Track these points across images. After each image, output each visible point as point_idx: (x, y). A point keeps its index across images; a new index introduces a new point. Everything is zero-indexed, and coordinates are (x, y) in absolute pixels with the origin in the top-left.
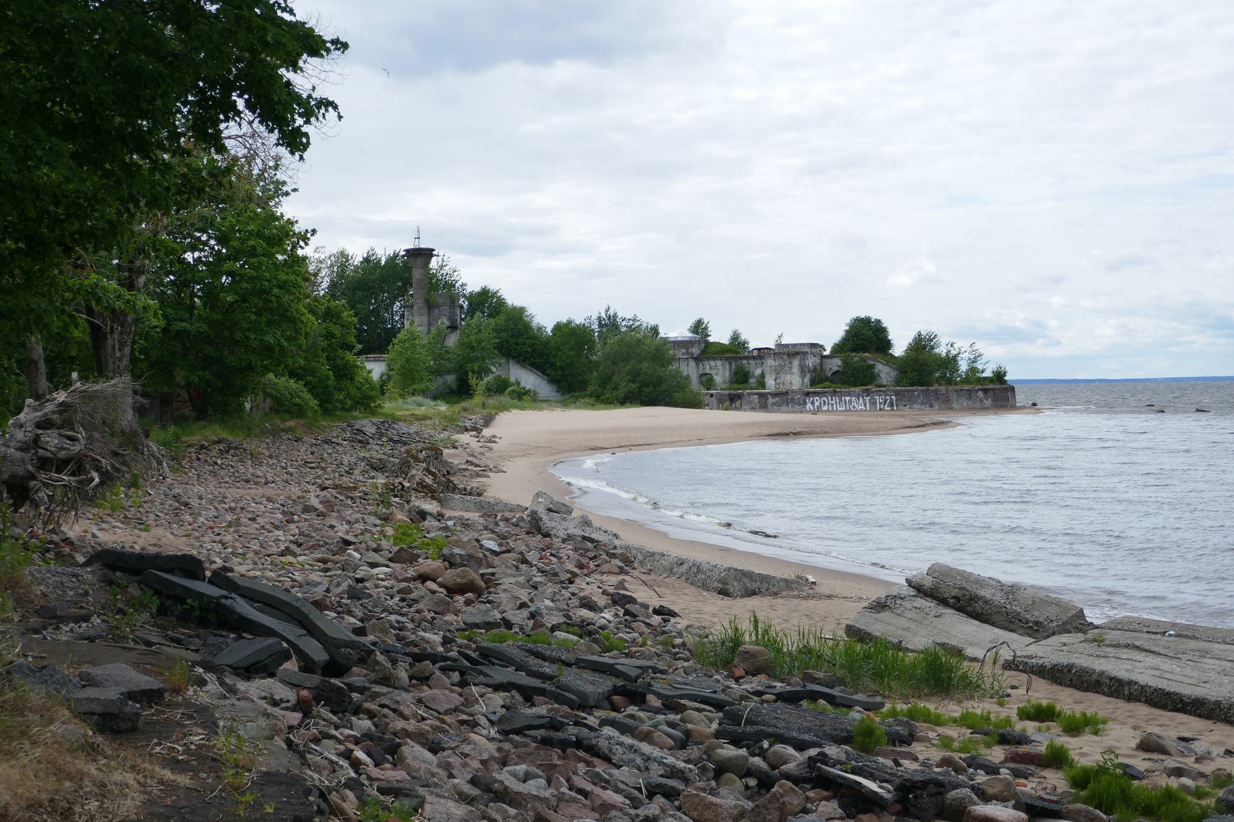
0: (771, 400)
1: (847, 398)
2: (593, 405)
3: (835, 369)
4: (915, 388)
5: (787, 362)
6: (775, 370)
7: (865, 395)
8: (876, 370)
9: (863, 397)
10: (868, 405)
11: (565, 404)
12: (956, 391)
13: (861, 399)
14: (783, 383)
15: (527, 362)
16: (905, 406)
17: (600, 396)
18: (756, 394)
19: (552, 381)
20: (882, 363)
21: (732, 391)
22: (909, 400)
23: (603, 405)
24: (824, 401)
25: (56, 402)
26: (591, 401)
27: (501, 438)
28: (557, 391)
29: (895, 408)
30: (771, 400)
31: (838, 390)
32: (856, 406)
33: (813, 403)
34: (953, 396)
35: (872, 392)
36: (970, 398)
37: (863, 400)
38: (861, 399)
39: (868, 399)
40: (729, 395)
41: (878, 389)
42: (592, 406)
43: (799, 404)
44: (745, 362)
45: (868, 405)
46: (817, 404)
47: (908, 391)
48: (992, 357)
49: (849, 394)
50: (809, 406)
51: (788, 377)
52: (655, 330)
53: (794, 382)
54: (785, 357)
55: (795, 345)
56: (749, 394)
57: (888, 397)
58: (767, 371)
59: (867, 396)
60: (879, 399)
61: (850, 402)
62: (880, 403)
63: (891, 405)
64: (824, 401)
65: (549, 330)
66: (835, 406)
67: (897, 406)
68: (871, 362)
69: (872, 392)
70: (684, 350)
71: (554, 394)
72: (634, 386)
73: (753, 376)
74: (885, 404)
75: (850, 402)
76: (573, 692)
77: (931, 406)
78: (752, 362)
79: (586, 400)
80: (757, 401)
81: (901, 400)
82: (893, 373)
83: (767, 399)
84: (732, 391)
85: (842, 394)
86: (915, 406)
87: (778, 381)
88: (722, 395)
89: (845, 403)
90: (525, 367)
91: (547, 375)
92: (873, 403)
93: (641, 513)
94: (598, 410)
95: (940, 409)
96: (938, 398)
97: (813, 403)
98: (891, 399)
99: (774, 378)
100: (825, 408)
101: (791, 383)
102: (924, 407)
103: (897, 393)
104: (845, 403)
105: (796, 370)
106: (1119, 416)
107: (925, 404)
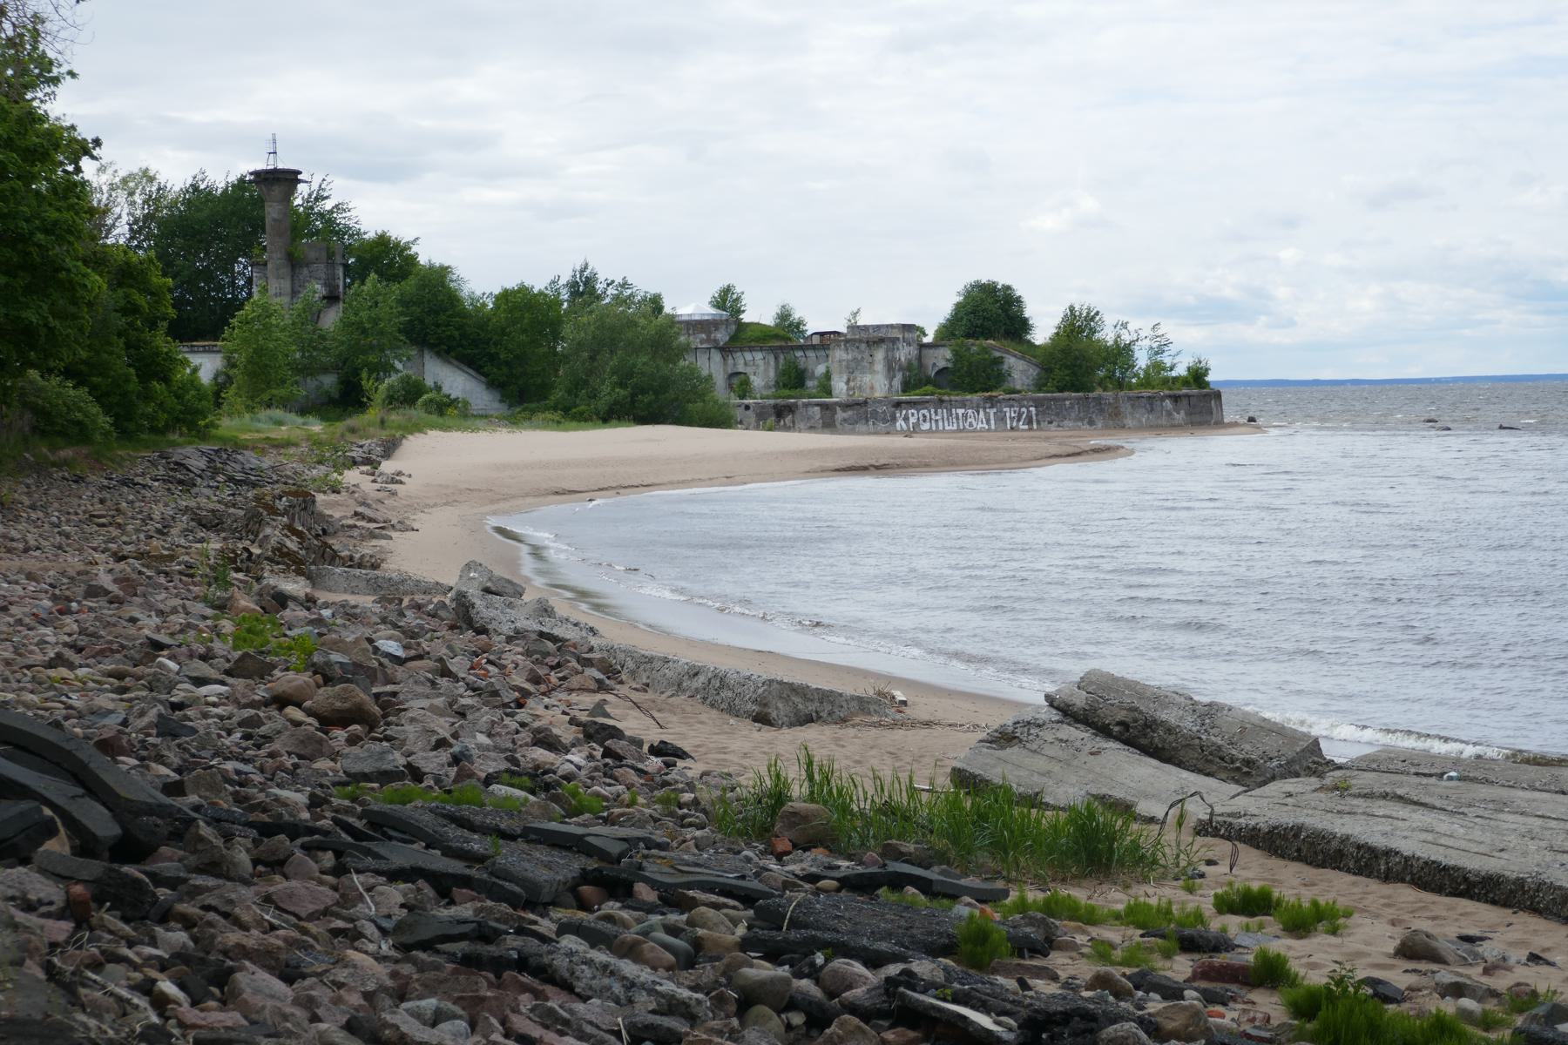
0: (840, 415)
1: (961, 411)
2: (559, 422)
3: (942, 364)
4: (1066, 394)
5: (866, 355)
6: (848, 368)
8: (1005, 367)
9: (985, 408)
10: (992, 422)
11: (513, 421)
12: (1129, 398)
14: (860, 388)
15: (453, 354)
16: (1050, 422)
17: (570, 409)
18: (817, 405)
19: (493, 384)
20: (1015, 356)
21: (779, 401)
22: (1057, 414)
23: (574, 424)
24: (924, 416)
26: (556, 416)
27: (410, 476)
28: (501, 401)
29: (1035, 426)
30: (840, 415)
31: (946, 398)
32: (974, 423)
33: (906, 419)
34: (1126, 407)
35: (999, 401)
37: (985, 413)
39: (992, 412)
40: (775, 406)
41: (1008, 396)
42: (558, 425)
43: (885, 421)
44: (799, 354)
45: (992, 422)
46: (912, 420)
47: (1054, 399)
49: (963, 405)
50: (900, 424)
51: (867, 378)
53: (877, 386)
54: (863, 346)
55: (879, 327)
56: (806, 405)
57: (1024, 409)
58: (835, 368)
60: (1009, 412)
61: (965, 416)
62: (1012, 419)
63: (1029, 421)
66: (940, 424)
68: (997, 354)
69: (999, 401)
71: (496, 405)
72: (623, 392)
73: (813, 377)
74: (1019, 420)
75: (965, 416)
77: (1091, 423)
78: (811, 354)
79: (548, 415)
80: (818, 416)
81: (1044, 413)
82: (1033, 372)
84: (779, 401)
85: (952, 405)
86: (1066, 423)
87: (852, 384)
88: (763, 407)
89: (957, 418)
90: (450, 363)
91: (485, 375)
92: (1001, 419)
94: (566, 430)
95: (1106, 427)
96: (1102, 411)
97: (906, 419)
98: (1029, 411)
99: (845, 378)
100: (926, 426)
101: (872, 388)
103: (1038, 403)
104: (957, 418)
105: (880, 366)
107: (1082, 420)
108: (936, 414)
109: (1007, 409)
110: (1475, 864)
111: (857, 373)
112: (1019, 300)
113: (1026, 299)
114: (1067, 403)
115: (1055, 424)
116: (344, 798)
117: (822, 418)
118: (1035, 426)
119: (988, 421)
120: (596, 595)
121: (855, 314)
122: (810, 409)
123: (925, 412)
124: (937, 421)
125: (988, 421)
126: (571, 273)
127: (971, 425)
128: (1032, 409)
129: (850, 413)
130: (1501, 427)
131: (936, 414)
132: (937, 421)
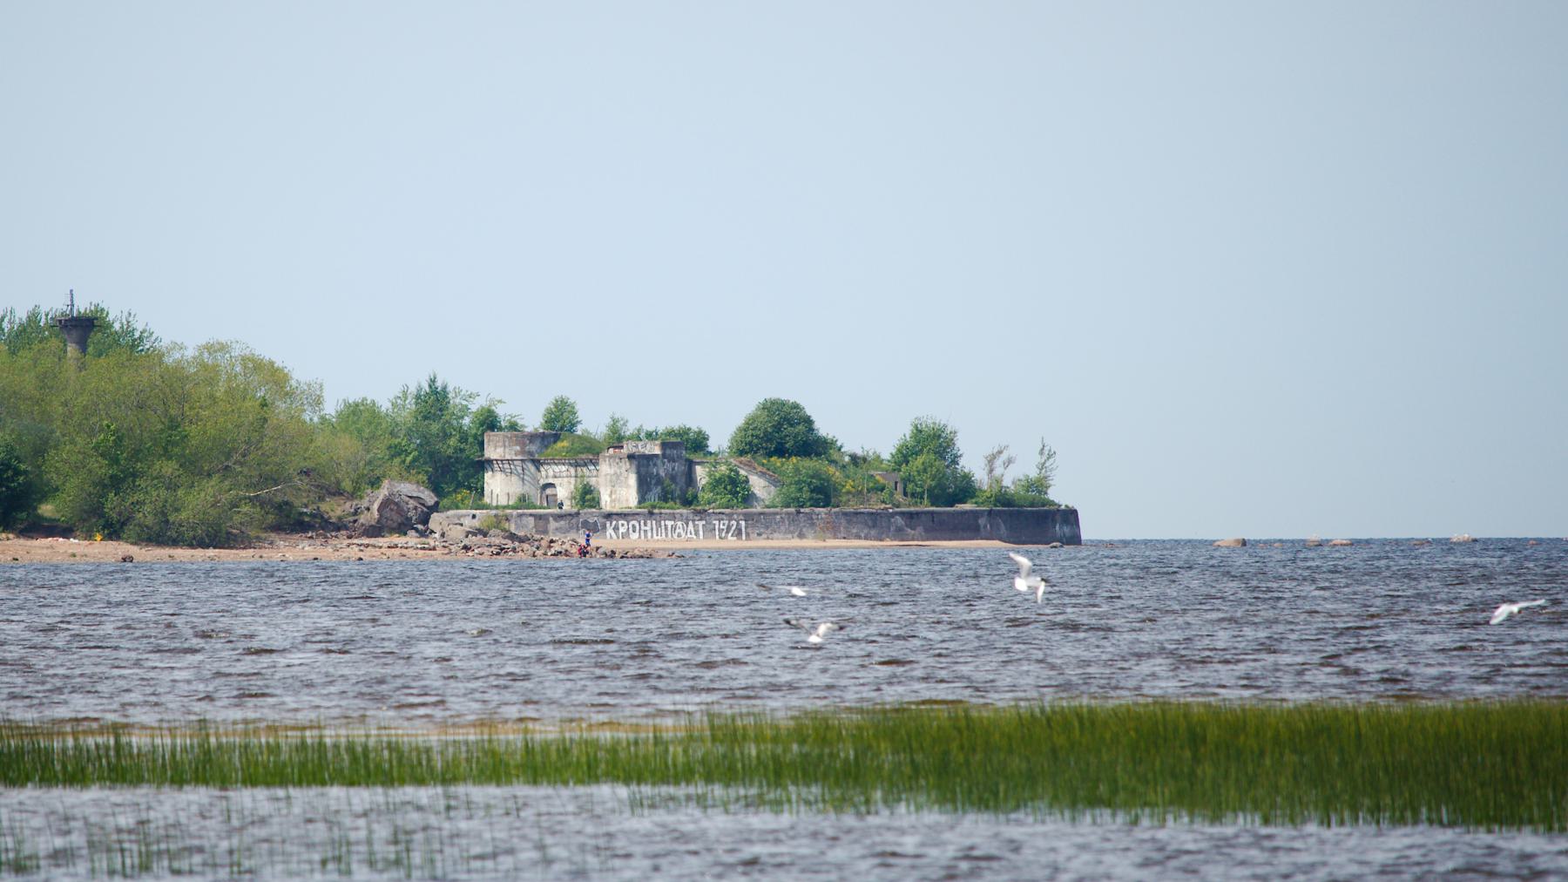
1: (669, 523)
7: (697, 518)
9: (693, 521)
10: (701, 533)
13: (690, 523)
18: (531, 515)
24: (634, 526)
25: (588, 693)
29: (744, 537)
32: (683, 535)
33: (616, 529)
36: (874, 526)
38: (690, 523)
39: (701, 523)
45: (701, 533)
46: (622, 530)
48: (995, 451)
49: (673, 517)
52: (483, 408)
57: (734, 522)
59: (701, 520)
61: (674, 528)
64: (634, 526)
65: (331, 408)
66: (649, 534)
67: (748, 535)
69: (709, 514)
70: (518, 448)
74: (727, 532)
76: (102, 731)
81: (753, 526)
83: (548, 522)
86: (775, 535)
89: (666, 529)
93: (1282, 833)
96: (813, 524)
97: (616, 529)
99: (609, 492)
101: (627, 500)
102: (790, 536)
104: (666, 529)
106: (336, 498)
107: (792, 533)
108: (645, 525)
109: (717, 522)
110: (939, 698)
111: (617, 488)
112: (796, 406)
113: (802, 403)
114: (778, 517)
115: (764, 536)
116: (841, 606)
117: (535, 526)
118: (744, 537)
119: (697, 533)
120: (1328, 541)
121: (500, 401)
122: (524, 518)
123: (634, 522)
124: (645, 531)
125: (697, 533)
126: (397, 391)
127: (679, 535)
128: (743, 523)
129: (562, 523)
130: (650, 557)
131: (645, 525)
132: (645, 531)
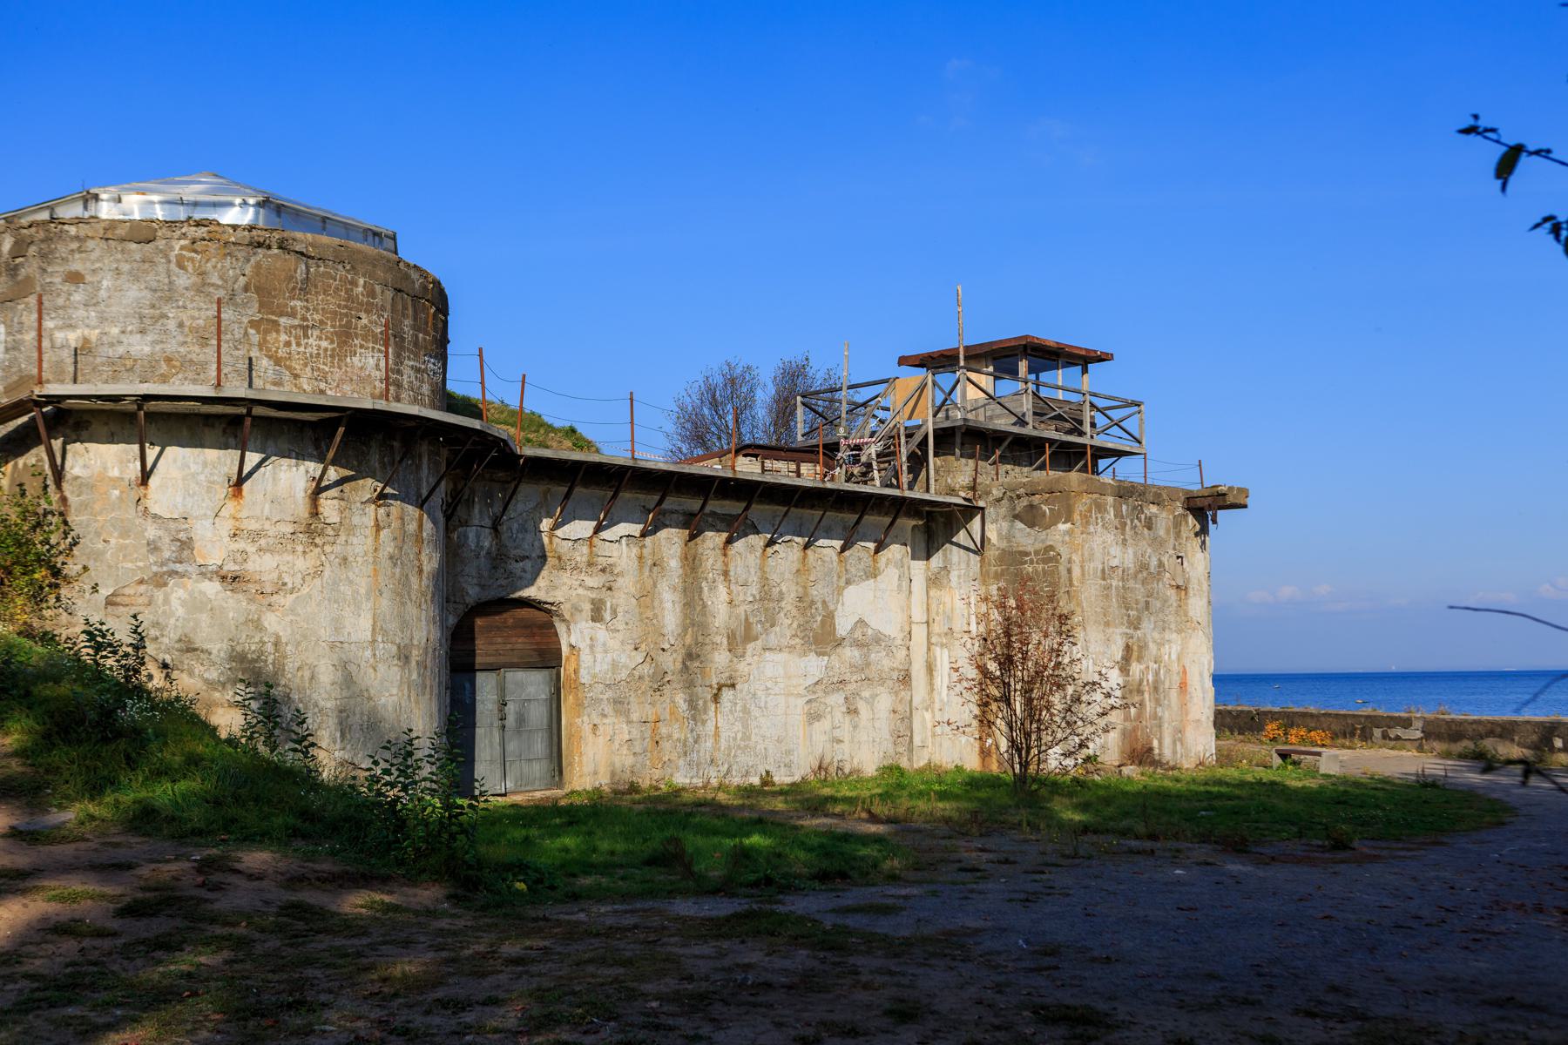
99: (513, 562)
